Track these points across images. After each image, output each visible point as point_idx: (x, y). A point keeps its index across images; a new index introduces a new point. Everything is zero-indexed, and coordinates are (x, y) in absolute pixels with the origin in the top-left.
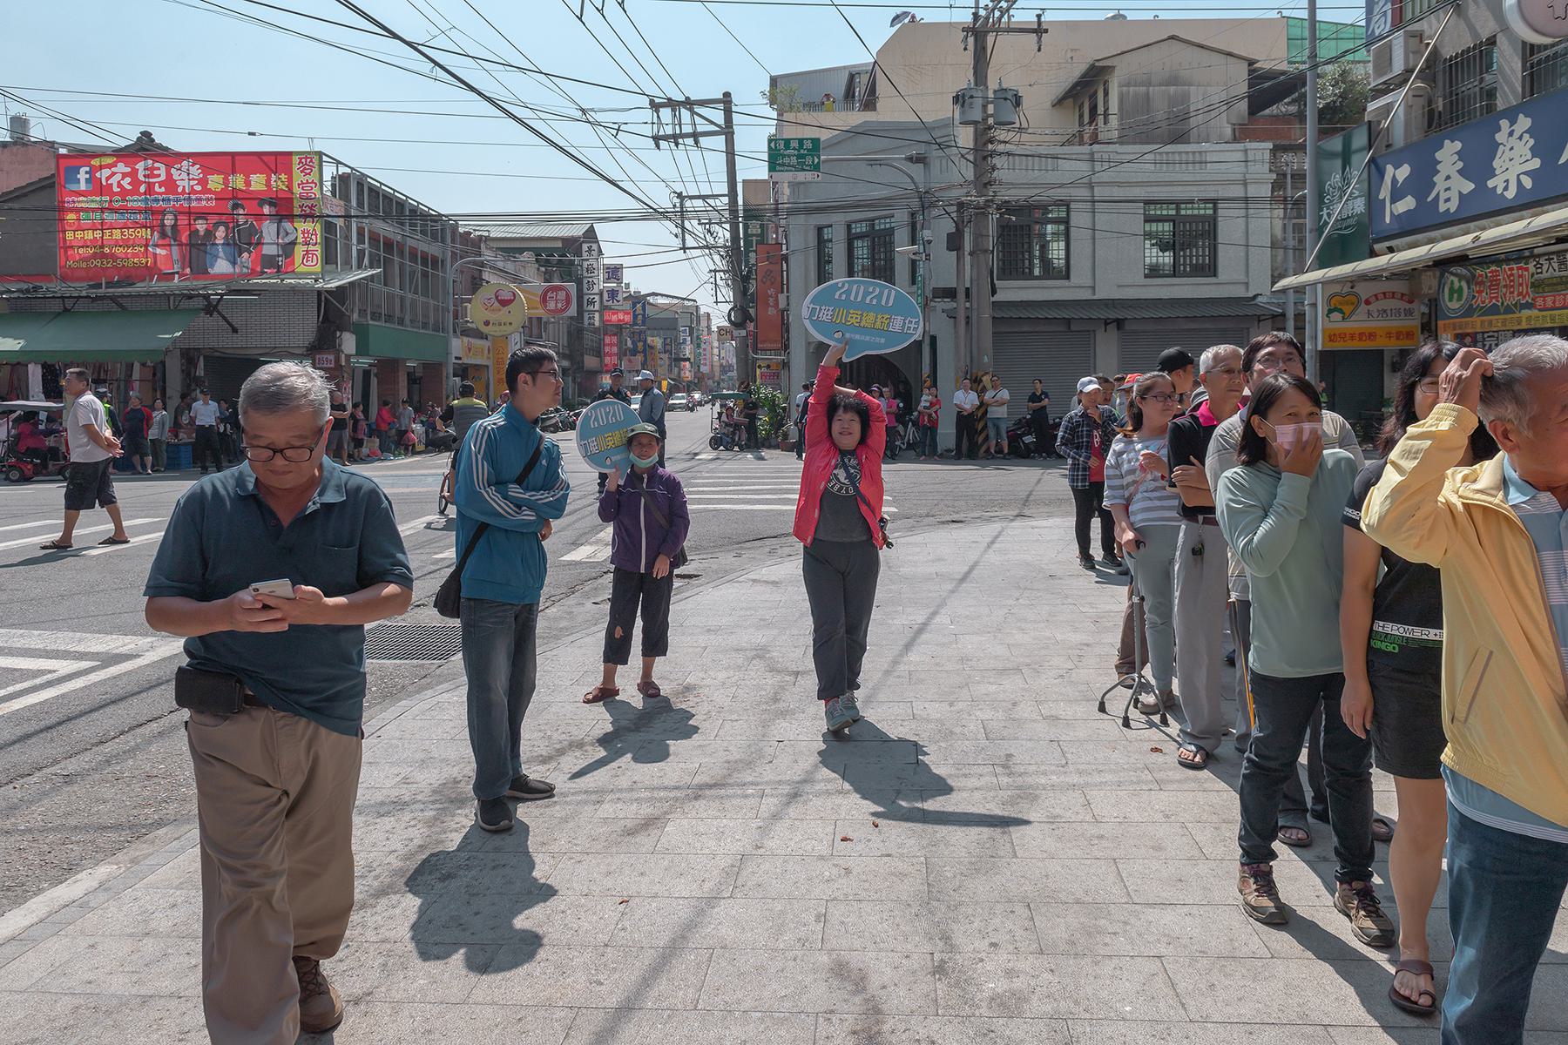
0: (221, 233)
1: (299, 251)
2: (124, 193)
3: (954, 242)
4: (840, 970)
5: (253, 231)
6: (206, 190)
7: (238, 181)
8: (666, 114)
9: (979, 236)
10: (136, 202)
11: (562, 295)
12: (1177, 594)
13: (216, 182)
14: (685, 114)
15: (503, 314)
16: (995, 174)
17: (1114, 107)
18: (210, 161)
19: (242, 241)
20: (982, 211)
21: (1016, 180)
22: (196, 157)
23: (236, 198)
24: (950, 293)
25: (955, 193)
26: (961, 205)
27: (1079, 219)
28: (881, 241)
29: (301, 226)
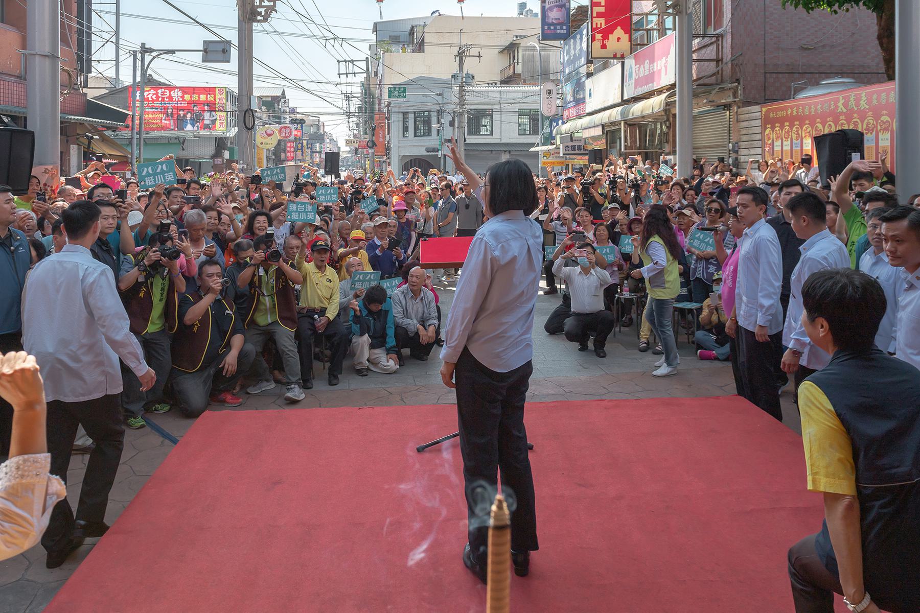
0: (189, 115)
1: (218, 122)
2: (153, 101)
3: (452, 124)
5: (201, 115)
6: (184, 100)
7: (195, 97)
8: (343, 65)
9: (460, 122)
10: (157, 104)
11: (288, 130)
13: (187, 97)
14: (351, 65)
15: (268, 140)
17: (520, 60)
18: (185, 90)
19: (197, 119)
20: (461, 114)
21: (473, 102)
22: (180, 88)
23: (196, 103)
24: (449, 141)
25: (453, 107)
26: (454, 112)
27: (496, 117)
28: (427, 122)
29: (219, 114)
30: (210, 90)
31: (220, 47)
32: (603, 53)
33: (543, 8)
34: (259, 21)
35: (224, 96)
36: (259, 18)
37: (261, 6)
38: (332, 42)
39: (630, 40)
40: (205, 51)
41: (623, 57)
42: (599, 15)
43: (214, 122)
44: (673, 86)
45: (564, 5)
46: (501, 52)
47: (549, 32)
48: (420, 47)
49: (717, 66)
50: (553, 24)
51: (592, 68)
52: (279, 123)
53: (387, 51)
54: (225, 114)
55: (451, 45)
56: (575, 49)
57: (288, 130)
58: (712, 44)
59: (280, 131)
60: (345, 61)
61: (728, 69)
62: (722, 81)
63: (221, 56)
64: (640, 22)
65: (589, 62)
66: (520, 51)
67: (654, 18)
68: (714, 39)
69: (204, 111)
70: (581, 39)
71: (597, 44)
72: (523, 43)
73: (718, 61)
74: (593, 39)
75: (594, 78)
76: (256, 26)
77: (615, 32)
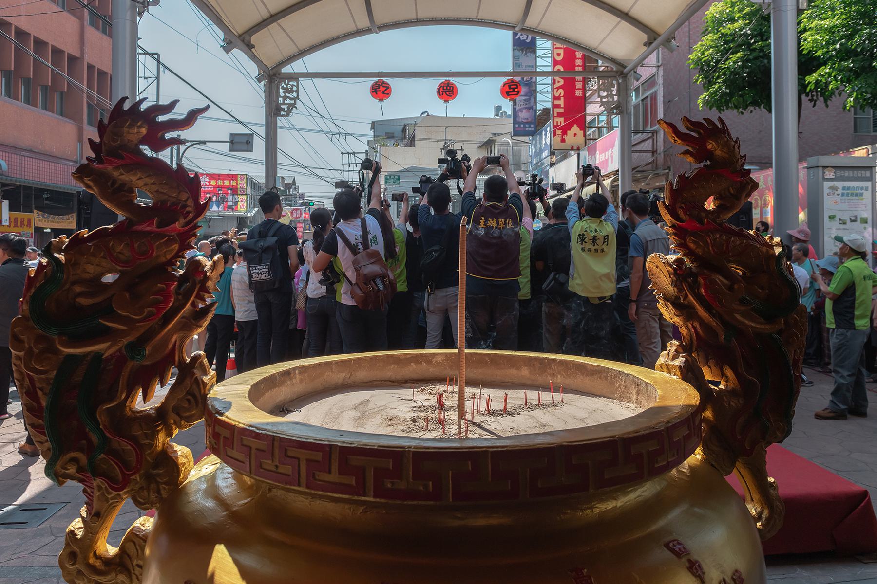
1: (239, 204)
4: (827, 106)
7: (220, 183)
8: (346, 156)
11: (298, 212)
12: (747, 322)
13: (213, 182)
16: (443, 156)
19: (222, 201)
22: (207, 175)
23: (222, 187)
29: (240, 197)
30: (233, 177)
31: (244, 139)
32: (563, 146)
33: (514, 110)
34: (283, 116)
35: (245, 181)
36: (282, 113)
37: (284, 104)
38: (337, 136)
39: (585, 135)
40: (232, 142)
41: (578, 149)
42: (560, 115)
43: (236, 203)
44: (618, 171)
45: (532, 108)
46: (480, 147)
47: (520, 129)
48: (411, 142)
49: (653, 155)
50: (524, 123)
51: (554, 159)
52: (290, 205)
53: (384, 145)
54: (245, 197)
55: (438, 140)
56: (541, 143)
57: (298, 212)
58: (649, 138)
59: (292, 213)
60: (348, 153)
61: (661, 158)
62: (657, 169)
63: (245, 146)
64: (593, 121)
65: (552, 154)
66: (496, 146)
67: (603, 118)
68: (650, 135)
69: (227, 194)
70: (546, 135)
71: (558, 139)
72: (498, 139)
73: (654, 152)
74: (554, 134)
75: (556, 166)
76: (281, 121)
77: (573, 128)
